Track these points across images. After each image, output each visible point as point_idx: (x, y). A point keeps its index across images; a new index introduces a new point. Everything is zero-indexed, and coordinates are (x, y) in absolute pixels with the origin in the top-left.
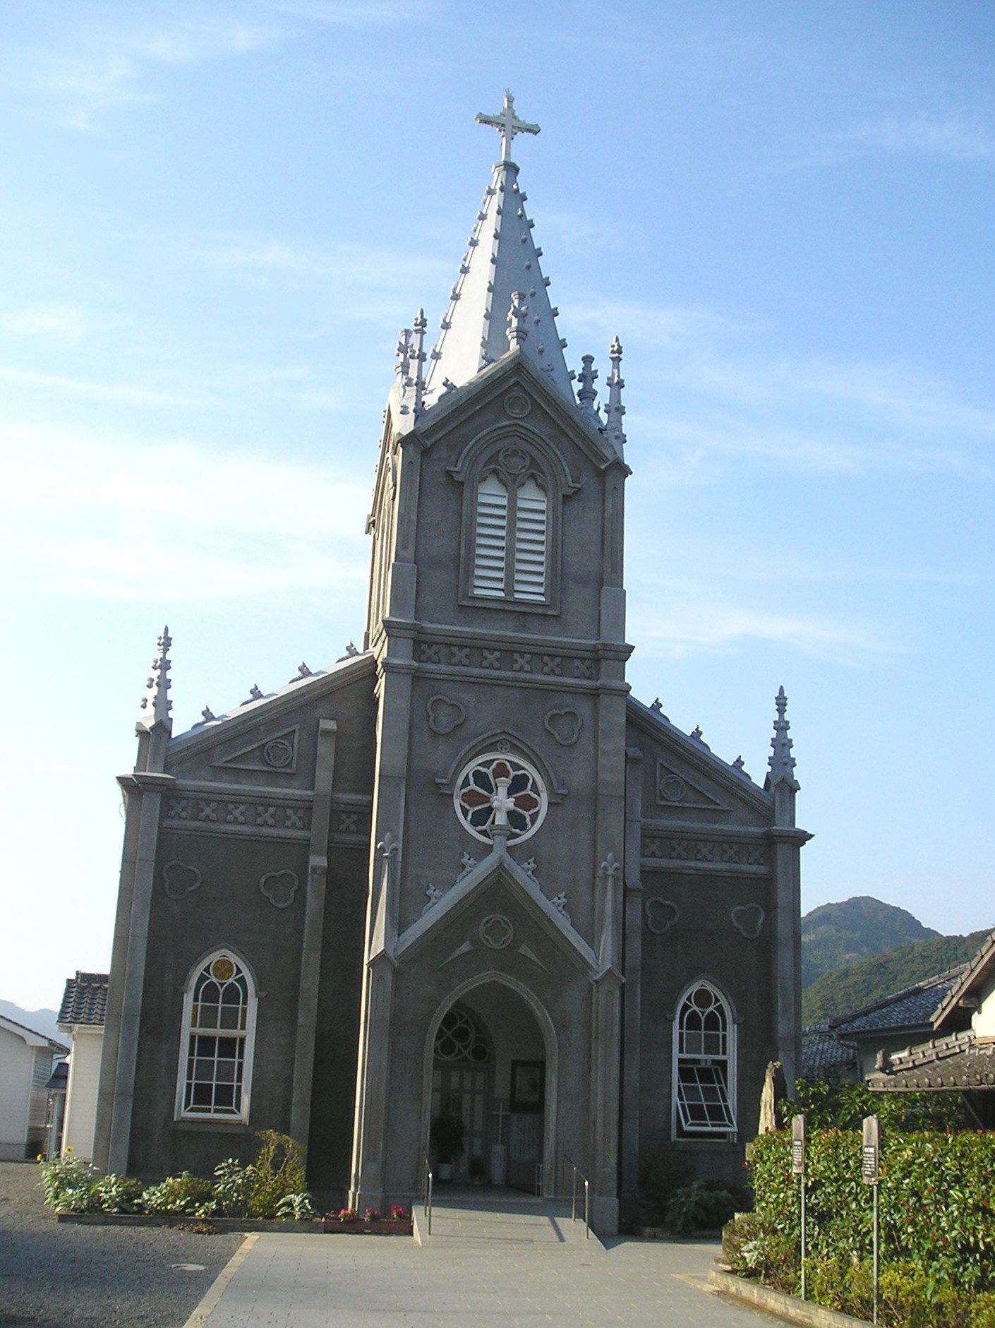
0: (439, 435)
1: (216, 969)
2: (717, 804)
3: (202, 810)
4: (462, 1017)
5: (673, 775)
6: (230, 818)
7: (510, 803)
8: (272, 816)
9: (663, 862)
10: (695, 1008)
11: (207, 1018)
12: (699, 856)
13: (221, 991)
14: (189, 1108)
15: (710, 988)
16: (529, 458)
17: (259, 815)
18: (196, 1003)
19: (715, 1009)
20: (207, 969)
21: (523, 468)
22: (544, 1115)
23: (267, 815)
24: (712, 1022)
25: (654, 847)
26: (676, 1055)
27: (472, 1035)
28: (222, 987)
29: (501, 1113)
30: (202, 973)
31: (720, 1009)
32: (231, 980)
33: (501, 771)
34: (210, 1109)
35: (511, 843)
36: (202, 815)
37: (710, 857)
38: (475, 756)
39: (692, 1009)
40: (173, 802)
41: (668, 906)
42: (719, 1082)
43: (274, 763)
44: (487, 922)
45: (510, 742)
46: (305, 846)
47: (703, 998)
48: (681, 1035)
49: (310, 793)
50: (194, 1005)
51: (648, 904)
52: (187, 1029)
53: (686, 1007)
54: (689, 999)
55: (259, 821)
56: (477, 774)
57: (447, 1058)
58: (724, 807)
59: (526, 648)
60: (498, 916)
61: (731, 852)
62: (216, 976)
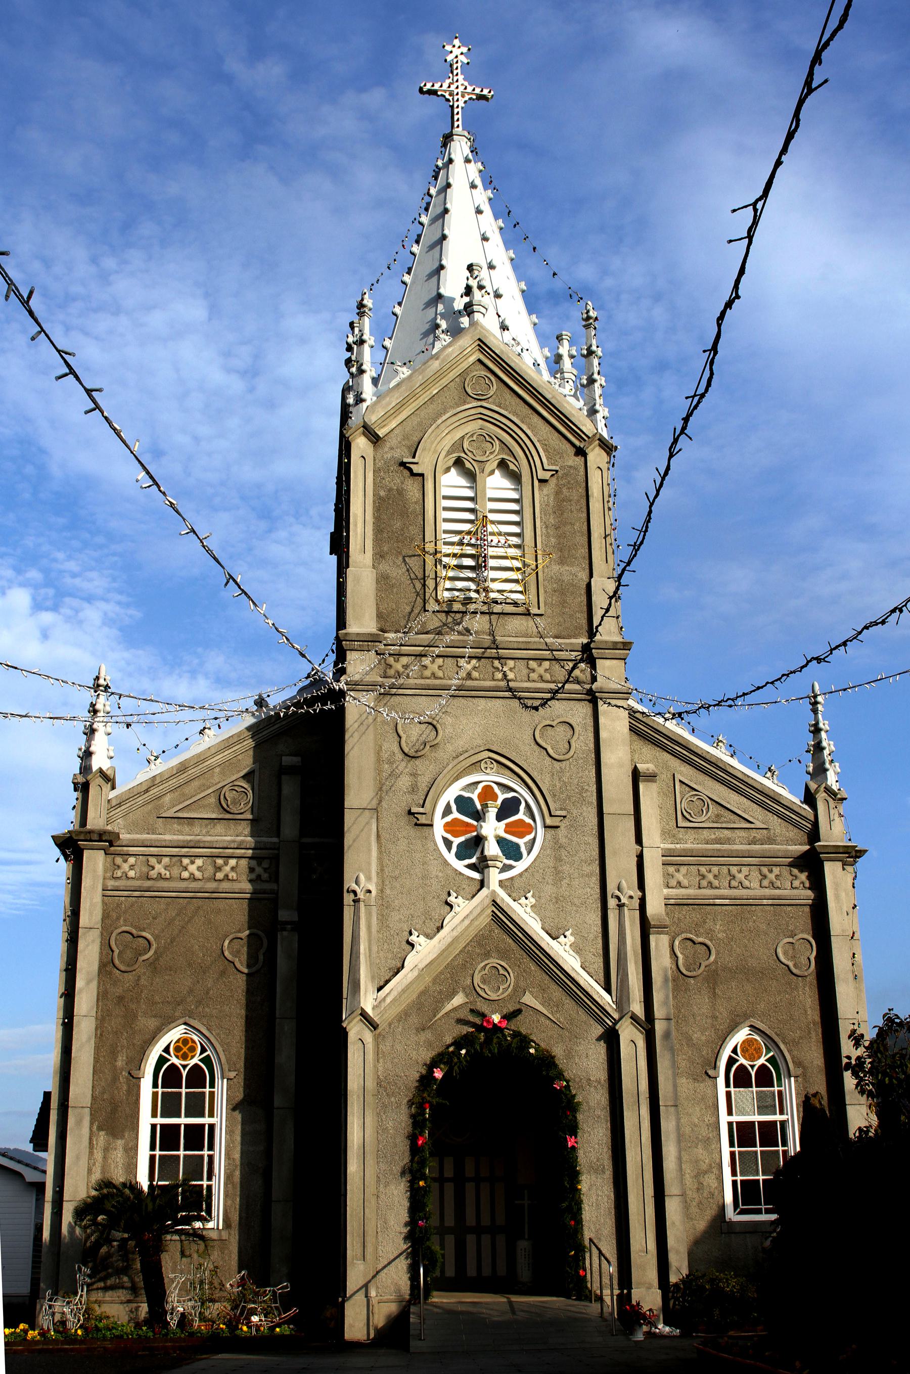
0: (393, 424)
1: (177, 1049)
5: (697, 793)
6: (185, 875)
8: (233, 869)
11: (169, 1106)
13: (184, 1074)
14: (738, 1210)
16: (497, 442)
17: (219, 869)
18: (155, 1090)
19: (766, 1060)
20: (167, 1050)
21: (491, 453)
23: (228, 868)
25: (680, 877)
26: (724, 1119)
28: (184, 1070)
30: (161, 1056)
32: (195, 1061)
33: (488, 794)
34: (736, 1176)
36: (153, 874)
38: (457, 779)
39: (737, 1064)
42: (780, 1085)
43: (234, 810)
44: (484, 968)
45: (441, 678)
49: (275, 840)
50: (153, 1093)
51: (677, 943)
52: (146, 1120)
53: (731, 1061)
54: (734, 1051)
55: (220, 875)
60: (493, 961)
61: (772, 876)
62: (177, 1057)
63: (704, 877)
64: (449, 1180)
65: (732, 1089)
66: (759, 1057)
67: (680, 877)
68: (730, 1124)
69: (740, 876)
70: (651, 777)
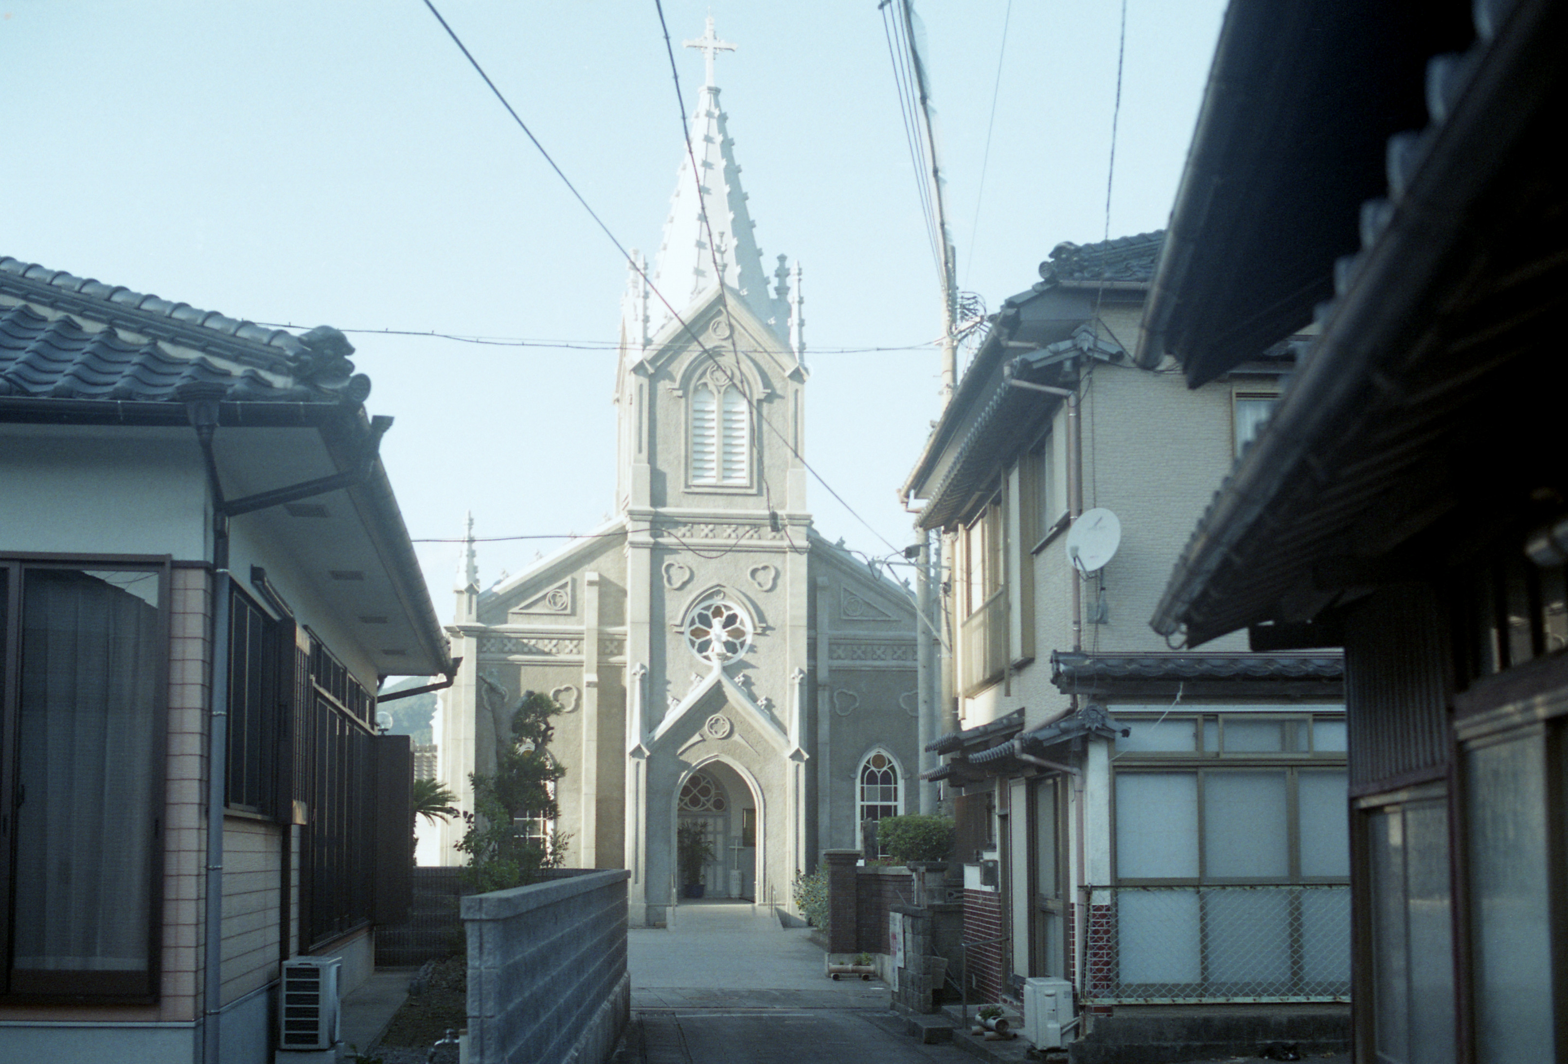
2: (887, 615)
3: (506, 645)
4: (704, 779)
7: (725, 637)
9: (847, 663)
10: (873, 768)
12: (875, 657)
15: (884, 753)
22: (1043, 461)
24: (887, 778)
25: (840, 652)
26: (859, 803)
27: (713, 792)
29: (736, 847)
31: (892, 768)
35: (727, 663)
36: (506, 649)
37: (883, 656)
40: (485, 641)
41: (851, 695)
46: (580, 664)
47: (879, 760)
48: (862, 789)
51: (835, 694)
53: (866, 768)
54: (868, 762)
56: (700, 616)
57: (695, 809)
58: (894, 618)
59: (733, 521)
63: (855, 652)
64: (711, 833)
65: (865, 786)
66: (883, 766)
67: (840, 652)
68: (862, 807)
69: (879, 652)
70: (824, 588)
